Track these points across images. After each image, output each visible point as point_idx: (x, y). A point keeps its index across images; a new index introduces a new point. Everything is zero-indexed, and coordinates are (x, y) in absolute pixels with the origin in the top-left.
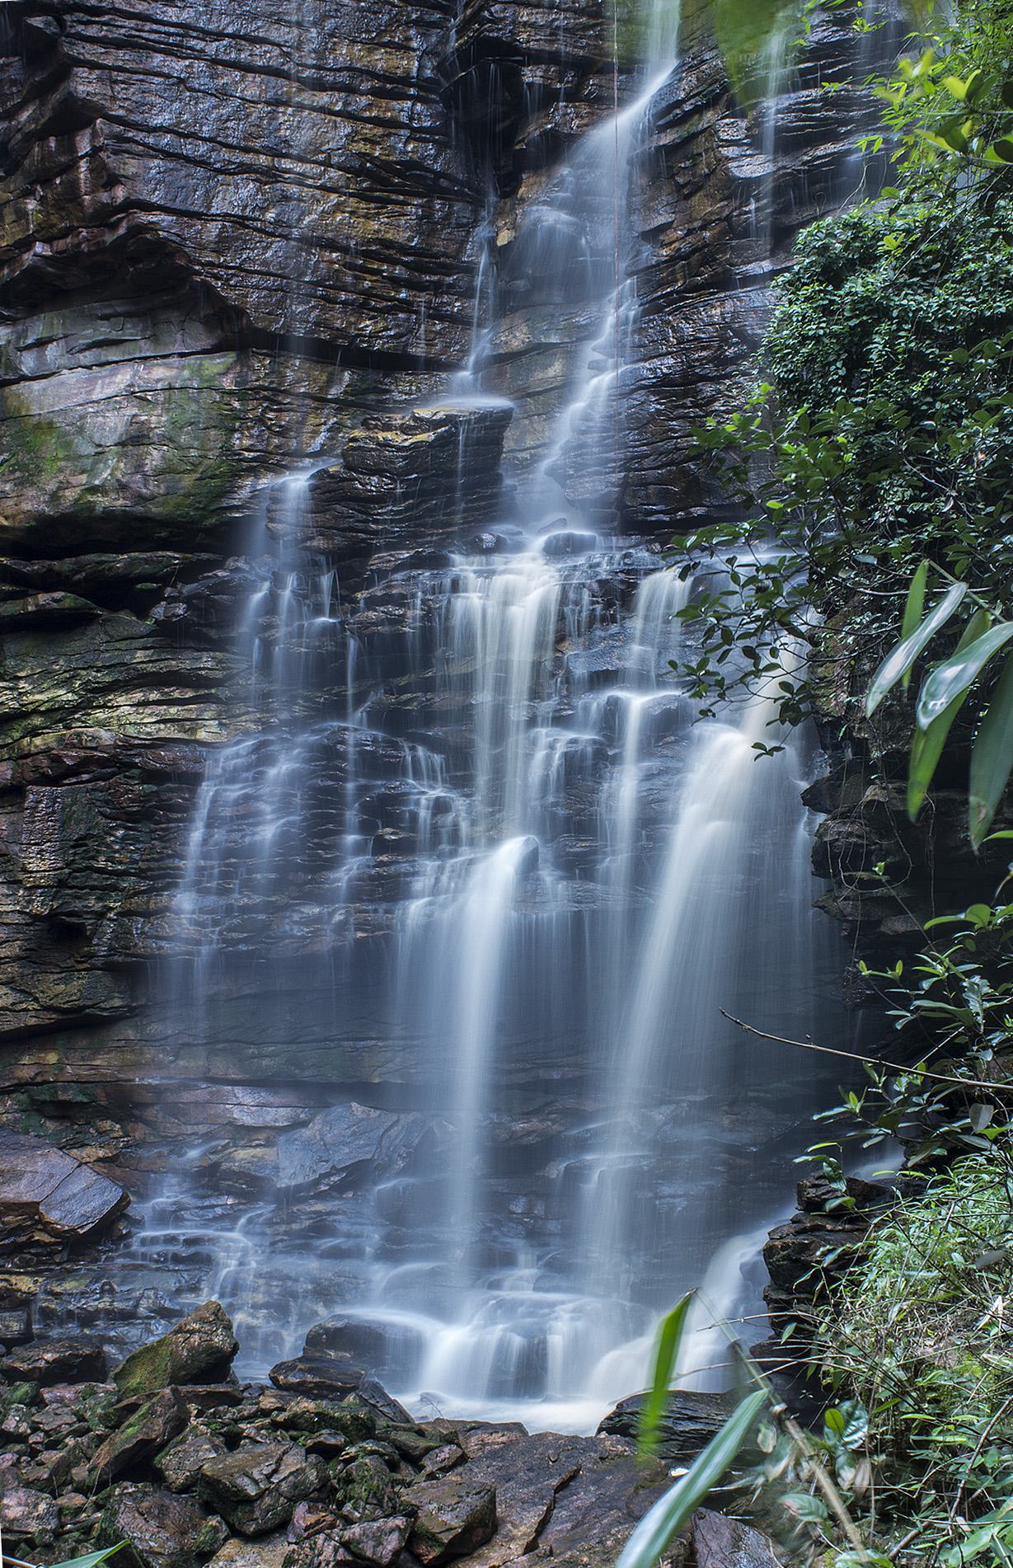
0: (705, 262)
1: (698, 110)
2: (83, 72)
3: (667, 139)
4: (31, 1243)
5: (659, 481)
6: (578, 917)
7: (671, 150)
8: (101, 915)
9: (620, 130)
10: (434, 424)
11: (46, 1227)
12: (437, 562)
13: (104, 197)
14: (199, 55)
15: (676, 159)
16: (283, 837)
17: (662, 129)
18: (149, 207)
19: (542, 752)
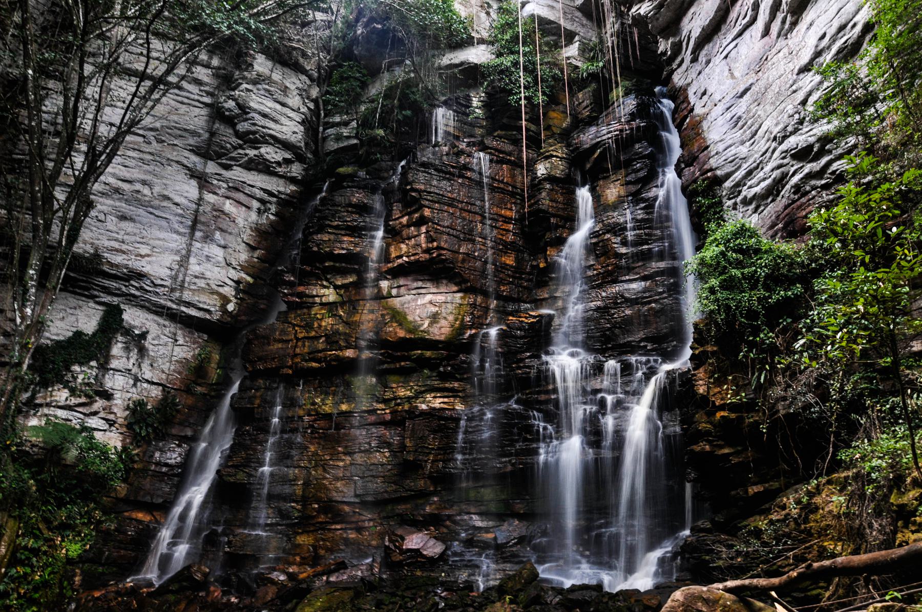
0: (609, 275)
1: (604, 234)
2: (427, 209)
3: (594, 241)
4: (417, 561)
5: (598, 337)
6: (596, 459)
7: (595, 244)
8: (426, 461)
9: (578, 238)
10: (534, 317)
11: (424, 556)
12: (539, 357)
13: (430, 245)
14: (457, 207)
15: (597, 248)
16: (491, 437)
17: (591, 238)
18: (444, 249)
19: (579, 412)
